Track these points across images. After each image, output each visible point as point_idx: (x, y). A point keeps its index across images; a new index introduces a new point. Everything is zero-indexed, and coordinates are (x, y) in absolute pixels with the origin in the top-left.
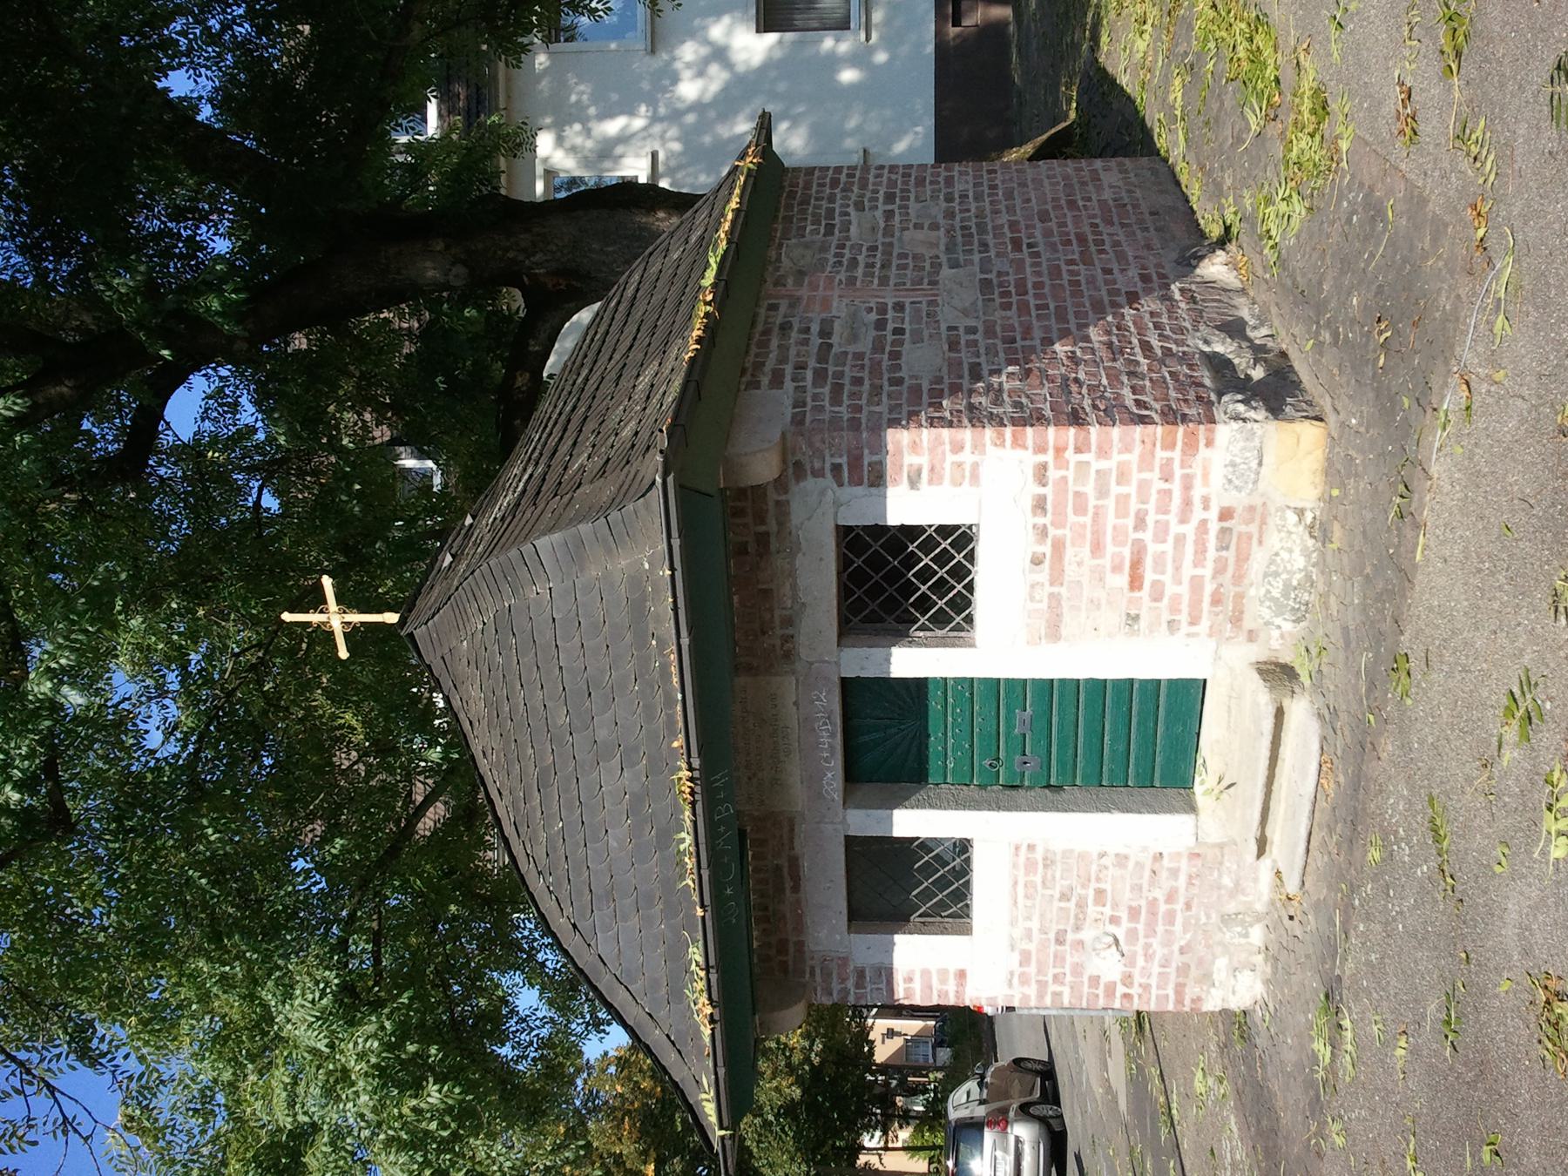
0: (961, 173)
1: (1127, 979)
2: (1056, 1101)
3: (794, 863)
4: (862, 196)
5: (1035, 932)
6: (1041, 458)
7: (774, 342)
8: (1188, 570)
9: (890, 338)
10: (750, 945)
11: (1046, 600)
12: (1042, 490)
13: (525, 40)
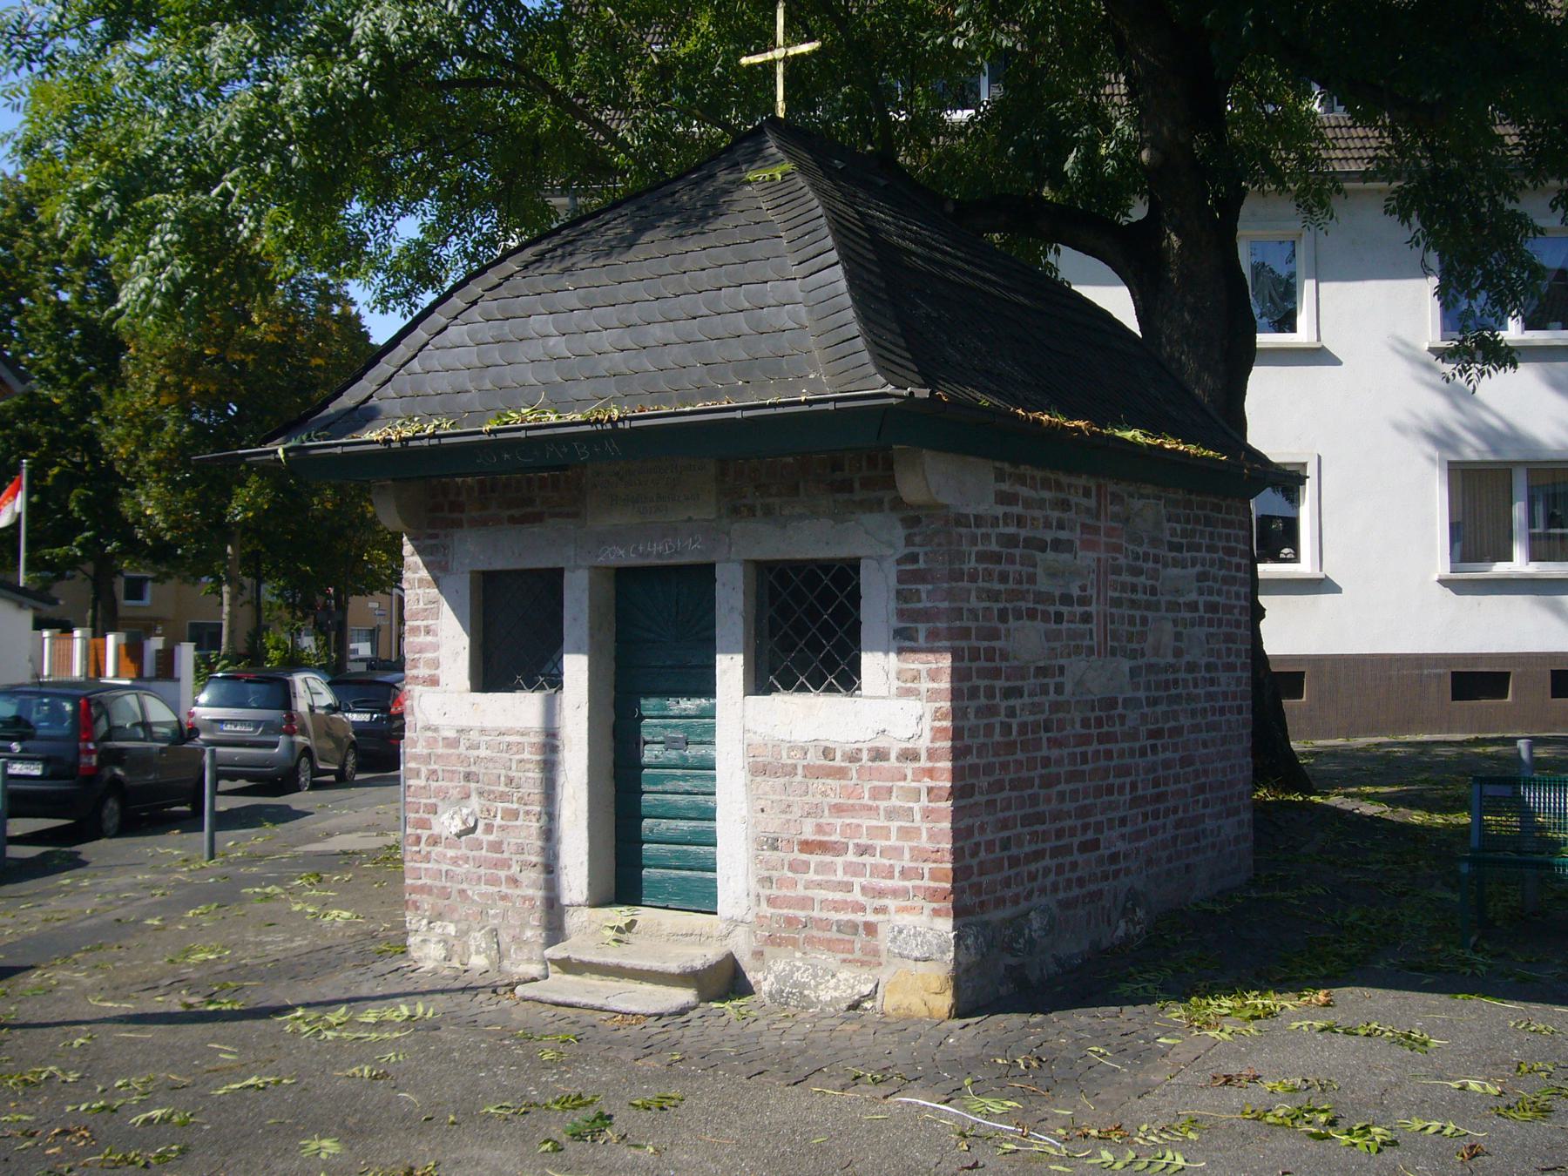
0: (1239, 679)
1: (434, 841)
2: (315, 786)
3: (537, 518)
4: (1215, 579)
5: (476, 753)
6: (924, 756)
7: (1046, 495)
9: (1052, 609)
10: (460, 475)
11: (789, 762)
13: (1414, 218)
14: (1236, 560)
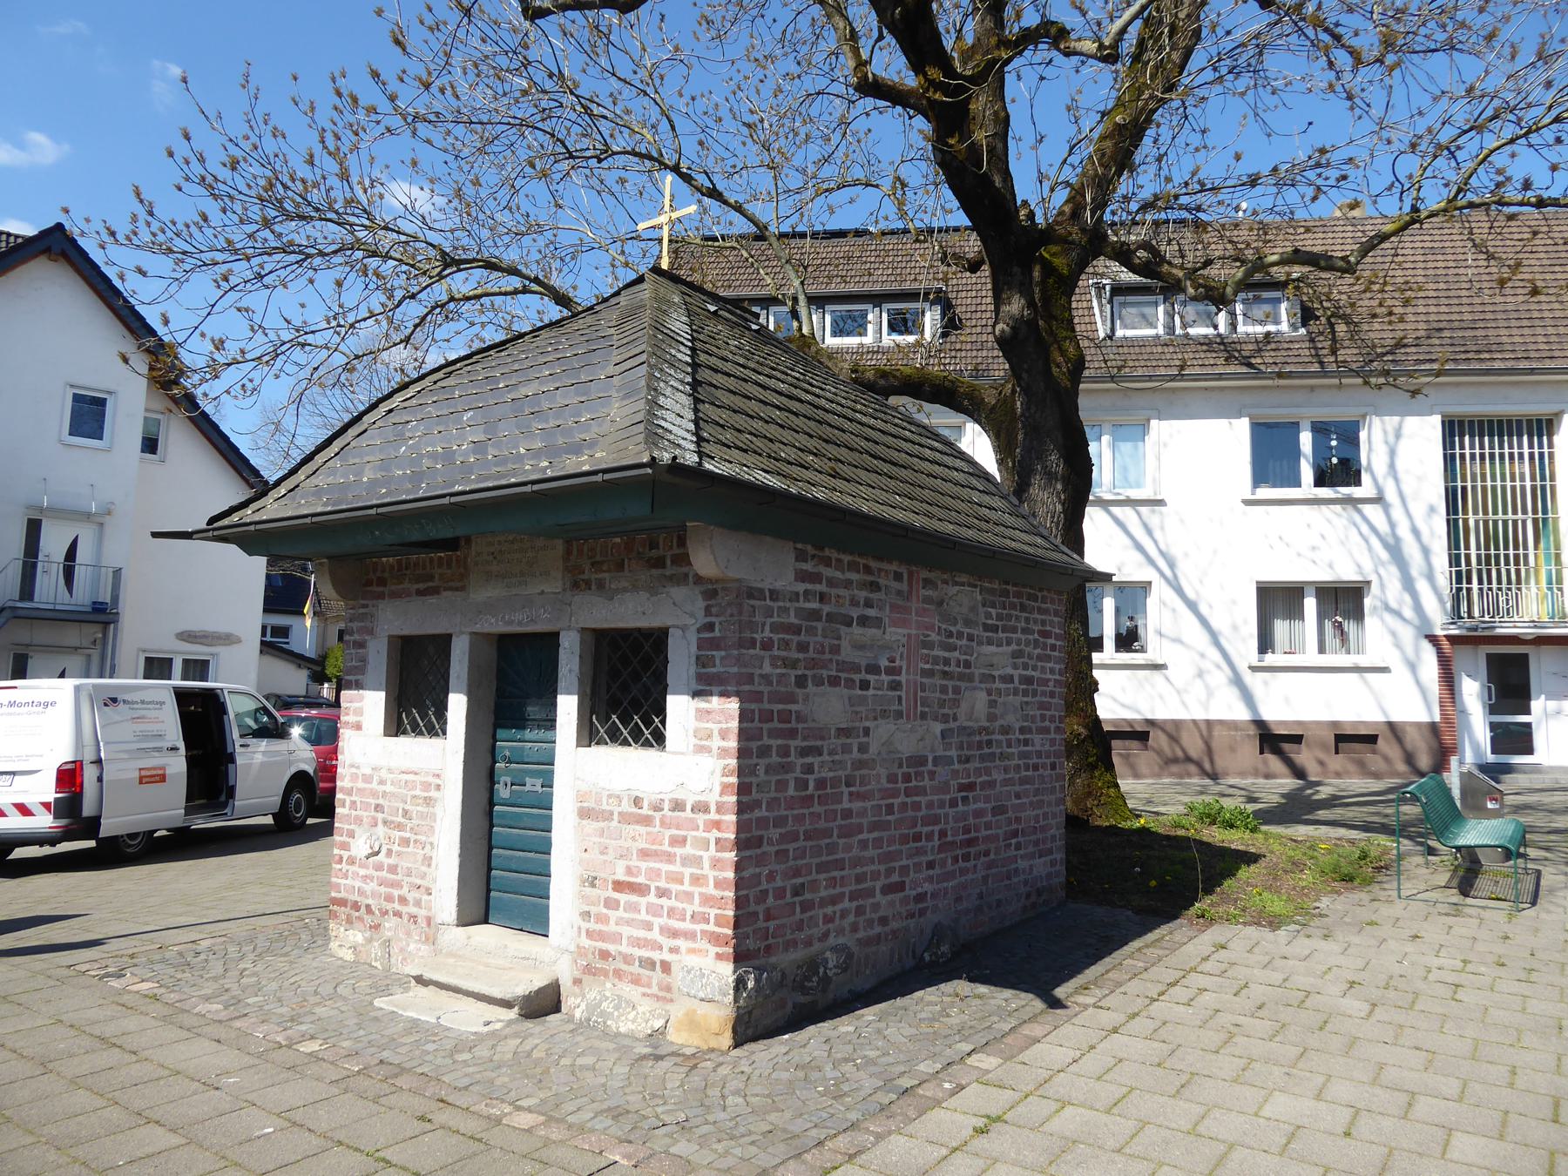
1: (352, 861)
3: (435, 591)
6: (713, 808)
7: (854, 576)
8: (626, 931)
12: (689, 808)
14: (1051, 641)
